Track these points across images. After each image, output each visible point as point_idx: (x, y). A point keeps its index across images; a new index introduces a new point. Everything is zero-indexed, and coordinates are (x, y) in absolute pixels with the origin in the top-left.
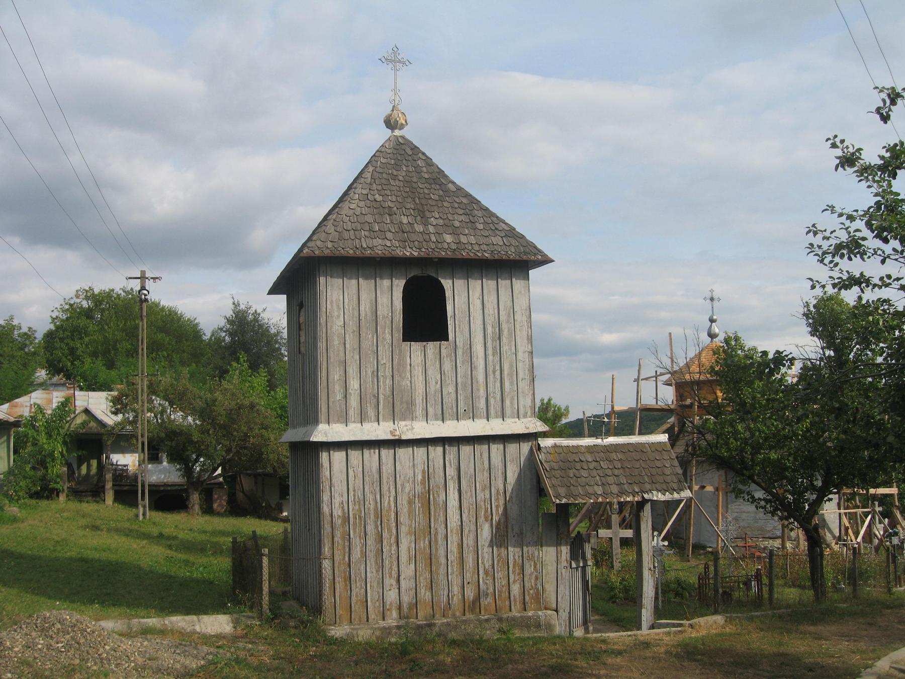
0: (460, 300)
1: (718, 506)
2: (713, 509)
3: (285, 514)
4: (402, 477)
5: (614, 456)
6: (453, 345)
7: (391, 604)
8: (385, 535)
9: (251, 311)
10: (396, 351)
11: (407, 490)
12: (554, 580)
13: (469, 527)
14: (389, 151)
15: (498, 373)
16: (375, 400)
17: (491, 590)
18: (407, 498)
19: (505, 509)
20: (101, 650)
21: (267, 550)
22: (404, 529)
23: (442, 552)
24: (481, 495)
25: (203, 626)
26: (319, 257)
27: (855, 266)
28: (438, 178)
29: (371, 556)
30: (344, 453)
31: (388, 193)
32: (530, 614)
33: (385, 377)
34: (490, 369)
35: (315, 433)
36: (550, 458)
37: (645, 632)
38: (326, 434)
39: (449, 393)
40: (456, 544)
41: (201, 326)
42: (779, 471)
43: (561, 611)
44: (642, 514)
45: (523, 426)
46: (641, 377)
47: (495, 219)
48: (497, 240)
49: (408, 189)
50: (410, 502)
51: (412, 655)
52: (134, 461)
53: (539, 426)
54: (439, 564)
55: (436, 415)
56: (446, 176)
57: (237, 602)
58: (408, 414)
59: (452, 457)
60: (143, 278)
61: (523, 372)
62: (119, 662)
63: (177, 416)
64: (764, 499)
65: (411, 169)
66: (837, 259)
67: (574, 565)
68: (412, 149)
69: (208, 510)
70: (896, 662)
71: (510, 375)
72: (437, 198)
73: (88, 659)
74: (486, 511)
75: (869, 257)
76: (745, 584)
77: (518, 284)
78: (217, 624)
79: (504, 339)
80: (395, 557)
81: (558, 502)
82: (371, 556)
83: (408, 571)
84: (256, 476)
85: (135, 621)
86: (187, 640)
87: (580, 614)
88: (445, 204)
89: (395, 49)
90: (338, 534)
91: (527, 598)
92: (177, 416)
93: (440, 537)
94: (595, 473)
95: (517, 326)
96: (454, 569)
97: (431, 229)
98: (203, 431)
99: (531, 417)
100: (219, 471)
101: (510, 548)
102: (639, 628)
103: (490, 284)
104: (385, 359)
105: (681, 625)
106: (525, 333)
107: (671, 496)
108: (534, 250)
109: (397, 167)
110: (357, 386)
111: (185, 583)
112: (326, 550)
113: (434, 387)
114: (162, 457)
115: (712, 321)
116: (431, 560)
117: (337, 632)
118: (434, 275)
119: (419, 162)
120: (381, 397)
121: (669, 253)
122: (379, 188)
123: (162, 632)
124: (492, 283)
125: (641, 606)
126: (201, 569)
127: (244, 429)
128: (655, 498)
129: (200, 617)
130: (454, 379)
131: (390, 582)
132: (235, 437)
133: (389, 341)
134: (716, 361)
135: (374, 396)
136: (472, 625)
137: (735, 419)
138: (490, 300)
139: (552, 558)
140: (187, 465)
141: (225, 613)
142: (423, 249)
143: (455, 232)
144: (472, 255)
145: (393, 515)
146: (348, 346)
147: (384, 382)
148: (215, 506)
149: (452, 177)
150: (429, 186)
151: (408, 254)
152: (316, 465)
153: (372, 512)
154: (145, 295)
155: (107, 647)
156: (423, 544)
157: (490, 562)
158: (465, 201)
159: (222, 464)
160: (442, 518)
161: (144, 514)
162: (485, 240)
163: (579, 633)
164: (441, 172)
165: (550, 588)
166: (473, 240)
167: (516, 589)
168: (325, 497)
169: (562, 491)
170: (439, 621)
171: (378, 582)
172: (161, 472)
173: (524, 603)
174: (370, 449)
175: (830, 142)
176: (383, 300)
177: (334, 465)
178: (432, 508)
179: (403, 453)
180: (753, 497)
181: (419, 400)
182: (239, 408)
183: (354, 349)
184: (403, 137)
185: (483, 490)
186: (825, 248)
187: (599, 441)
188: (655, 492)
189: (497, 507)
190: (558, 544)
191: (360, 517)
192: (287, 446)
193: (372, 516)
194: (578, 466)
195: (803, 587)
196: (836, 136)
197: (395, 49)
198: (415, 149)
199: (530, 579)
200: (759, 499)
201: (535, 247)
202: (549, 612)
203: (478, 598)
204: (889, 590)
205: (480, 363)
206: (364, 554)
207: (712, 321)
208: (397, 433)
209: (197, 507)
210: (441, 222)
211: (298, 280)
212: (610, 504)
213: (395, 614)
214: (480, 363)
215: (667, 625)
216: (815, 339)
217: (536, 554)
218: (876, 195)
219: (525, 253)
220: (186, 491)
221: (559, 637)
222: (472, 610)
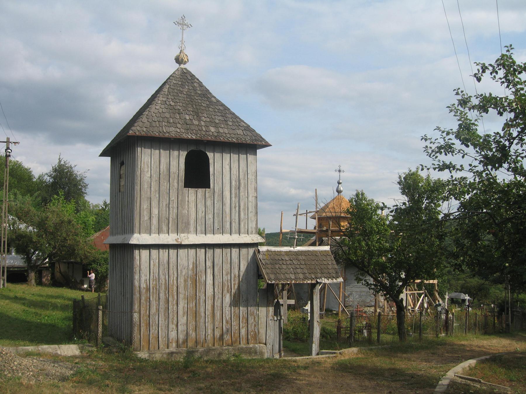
0: (218, 165)
1: (340, 287)
2: (337, 289)
3: (85, 286)
4: (181, 266)
5: (300, 257)
6: (212, 191)
7: (172, 339)
8: (170, 299)
10: (180, 193)
11: (183, 274)
12: (265, 328)
13: (218, 295)
14: (178, 77)
15: (237, 208)
16: (167, 221)
18: (183, 279)
19: (239, 286)
20: (12, 364)
21: (101, 307)
22: (181, 296)
23: (202, 310)
24: (225, 278)
25: (62, 351)
26: (138, 136)
27: (447, 159)
28: (206, 94)
29: (162, 311)
30: (148, 251)
31: (178, 101)
32: (251, 346)
33: (173, 208)
34: (233, 205)
35: (132, 239)
36: (265, 257)
37: (314, 356)
39: (210, 219)
40: (210, 305)
41: (33, 173)
42: (382, 268)
43: (268, 344)
44: (314, 291)
45: (250, 238)
46: (299, 213)
47: (238, 120)
48: (240, 132)
49: (189, 100)
50: (185, 281)
51: (190, 368)
55: (201, 230)
56: (210, 93)
57: (81, 337)
58: (186, 229)
60: (8, 142)
61: (251, 208)
62: (23, 371)
63: (23, 226)
64: (373, 284)
65: (191, 88)
66: (438, 154)
67: (275, 319)
68: (191, 76)
69: (39, 283)
70: (457, 373)
71: (244, 209)
72: (205, 105)
73: (5, 370)
74: (228, 287)
75: (456, 154)
76: (359, 331)
77: (251, 157)
78: (70, 350)
79: (242, 189)
80: (175, 312)
81: (270, 282)
82: (162, 311)
83: (183, 320)
84: (69, 263)
85: (20, 348)
86: (56, 359)
87: (277, 346)
88: (210, 109)
89: (183, 17)
90: (143, 298)
91: (249, 337)
92: (23, 226)
93: (202, 301)
94: (290, 267)
96: (209, 319)
97: (203, 123)
98: (39, 235)
99: (255, 234)
100: (47, 260)
102: (310, 354)
103: (235, 157)
104: (173, 197)
105: (335, 353)
106: (253, 186)
107: (332, 281)
108: (260, 139)
109: (182, 86)
111: (39, 326)
112: (136, 307)
113: (201, 214)
114: (11, 250)
115: (339, 183)
116: (196, 314)
117: (143, 355)
118: (203, 150)
119: (195, 84)
120: (171, 219)
122: (173, 98)
123: (39, 355)
124: (157, 151)
126: (46, 318)
127: (64, 235)
128: (323, 282)
129: (60, 346)
131: (172, 326)
132: (58, 239)
133: (176, 187)
134: (351, 206)
137: (356, 238)
138: (235, 166)
139: (265, 313)
140: (28, 256)
141: (74, 344)
143: (216, 126)
144: (226, 139)
145: (175, 288)
146: (152, 189)
147: (173, 211)
148: (44, 280)
149: (214, 94)
150: (201, 99)
151: (190, 137)
152: (132, 258)
154: (9, 153)
155: (16, 363)
156: (192, 305)
157: (230, 316)
158: (221, 108)
159: (49, 256)
160: (203, 290)
161: (4, 285)
162: (231, 132)
163: (277, 356)
164: (207, 91)
165: (262, 331)
166: (226, 131)
167: (243, 331)
168: (137, 277)
169: (272, 276)
171: (165, 327)
172: (11, 258)
173: (248, 340)
175: (456, 91)
176: (174, 163)
177: (142, 258)
178: (198, 284)
179: (182, 252)
180: (367, 283)
181: (192, 222)
182: (62, 223)
183: (156, 191)
184: (185, 69)
185: (227, 275)
186: (433, 148)
187: (292, 249)
188: (323, 279)
189: (234, 284)
190: (268, 305)
192: (108, 246)
194: (281, 262)
195: (394, 334)
196: (459, 89)
197: (183, 17)
198: (193, 76)
200: (371, 284)
201: (261, 137)
203: (222, 336)
204: (437, 335)
206: (158, 310)
207: (339, 183)
208: (180, 240)
209: (33, 281)
210: (208, 120)
211: (122, 149)
212: (277, 284)
213: (174, 345)
215: (327, 353)
216: (404, 196)
218: (459, 120)
219: (256, 140)
220: (27, 271)
221: (268, 359)
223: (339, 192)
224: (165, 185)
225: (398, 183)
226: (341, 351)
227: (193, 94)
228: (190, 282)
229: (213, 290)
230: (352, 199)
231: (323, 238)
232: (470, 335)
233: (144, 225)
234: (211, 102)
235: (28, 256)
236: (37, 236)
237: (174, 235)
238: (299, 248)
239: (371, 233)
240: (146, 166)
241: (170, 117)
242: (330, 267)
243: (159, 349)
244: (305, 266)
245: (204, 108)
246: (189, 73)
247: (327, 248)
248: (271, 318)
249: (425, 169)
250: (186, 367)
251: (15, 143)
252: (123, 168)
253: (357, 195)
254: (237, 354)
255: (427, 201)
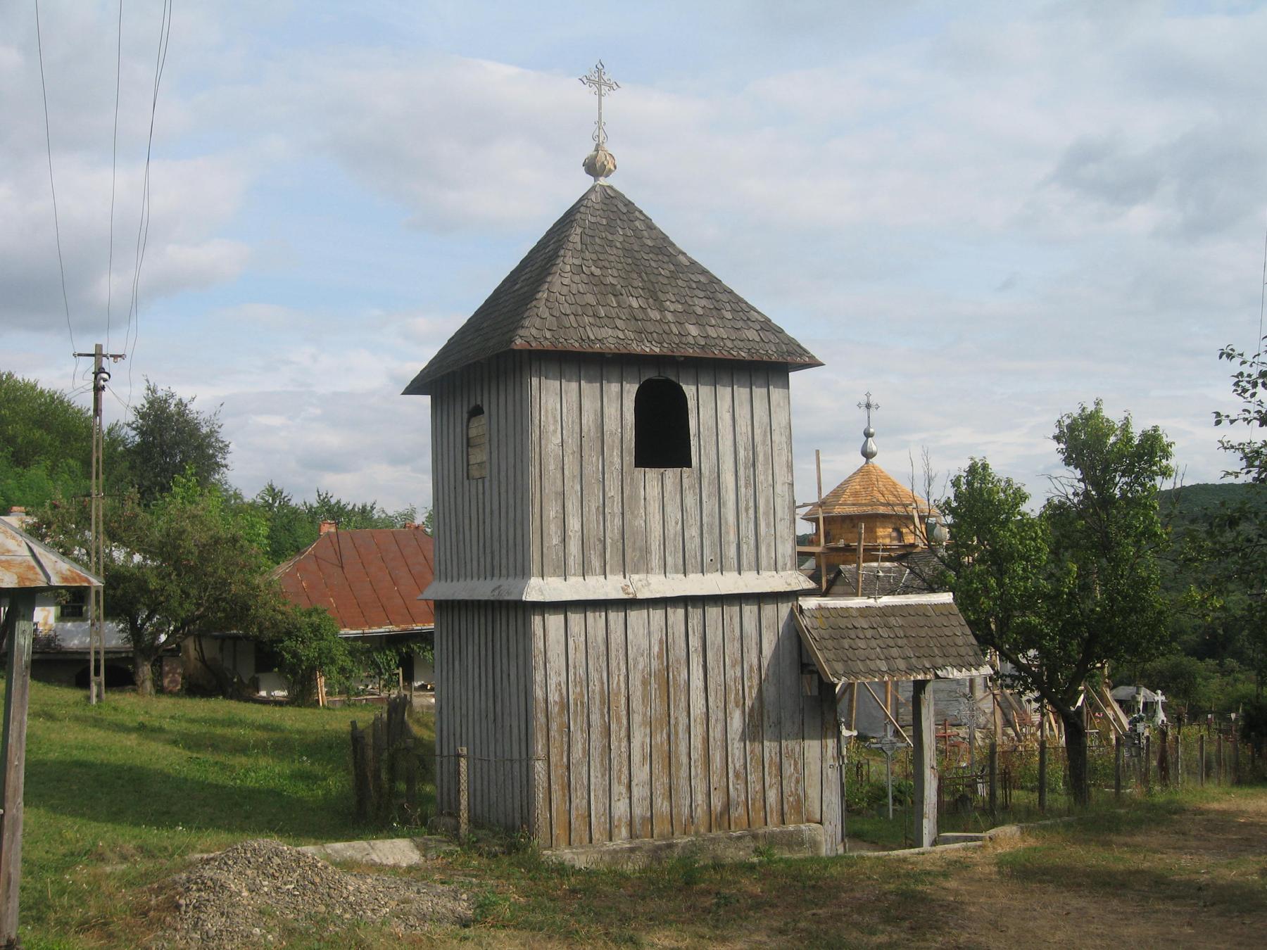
0: (706, 413)
5: (892, 621)
7: (620, 819)
8: (614, 727)
9: (173, 402)
10: (627, 481)
11: (640, 667)
14: (597, 206)
15: (751, 511)
16: (600, 546)
17: (743, 797)
19: (760, 690)
22: (637, 719)
24: (730, 673)
28: (663, 247)
30: (562, 617)
31: (607, 265)
32: (791, 827)
34: (742, 505)
36: (817, 623)
37: (926, 845)
38: (541, 590)
40: (700, 737)
43: (827, 823)
47: (744, 306)
48: (752, 334)
49: (630, 261)
50: (645, 683)
52: (46, 618)
53: (797, 580)
54: (679, 765)
55: (675, 566)
58: (643, 565)
59: (695, 622)
60: (98, 355)
64: (1010, 676)
65: (630, 233)
69: (160, 690)
71: (766, 514)
72: (668, 274)
74: (737, 694)
77: (776, 393)
79: (760, 467)
80: (625, 755)
84: (223, 639)
90: (554, 726)
91: (786, 807)
94: (874, 643)
95: (775, 449)
96: (698, 770)
97: (670, 317)
101: (766, 743)
102: (920, 844)
103: (742, 392)
104: (613, 491)
105: (977, 839)
106: (784, 459)
109: (610, 227)
110: (577, 527)
112: (540, 748)
113: (673, 528)
115: (868, 435)
118: (674, 379)
119: (637, 223)
120: (608, 541)
121: (945, 356)
124: (574, 385)
125: (921, 816)
129: (372, 842)
130: (698, 518)
131: (619, 789)
133: (618, 466)
135: (599, 540)
136: (722, 845)
138: (743, 413)
140: (133, 622)
142: (612, 335)
145: (623, 700)
147: (612, 522)
148: (166, 682)
149: (680, 245)
153: (597, 697)
154: (105, 380)
156: (660, 738)
158: (703, 279)
160: (683, 704)
161: (98, 696)
165: (813, 793)
167: (772, 796)
168: (539, 677)
170: (681, 840)
173: (782, 814)
174: (594, 612)
176: (611, 411)
178: (672, 690)
179: (636, 617)
181: (655, 546)
182: (216, 542)
184: (611, 187)
185: (733, 666)
187: (871, 602)
189: (750, 687)
190: (823, 736)
191: (582, 703)
193: (597, 702)
198: (629, 204)
199: (789, 782)
201: (799, 346)
202: (814, 825)
203: (727, 806)
205: (730, 497)
207: (868, 435)
209: (148, 684)
210: (680, 307)
213: (624, 832)
214: (730, 497)
215: (956, 840)
216: (1072, 468)
217: (797, 749)
219: (789, 353)
220: (131, 660)
222: (720, 827)
223: (868, 455)
224: (592, 460)
225: (1055, 437)
226: (992, 832)
227: (636, 248)
228: (654, 686)
229: (703, 702)
230: (958, 478)
231: (842, 567)
232: (1212, 788)
233: (552, 555)
234: (677, 264)
235: (133, 622)
236: (158, 576)
237: (616, 577)
238: (886, 600)
239: (1010, 557)
240: (551, 420)
241: (598, 303)
242: (960, 641)
243: (591, 841)
244: (905, 641)
245: (666, 281)
246: (619, 196)
247: (946, 598)
248: (831, 762)
249: (1225, 422)
250: (681, 881)
251: (115, 357)
252: (475, 422)
253: (972, 470)
254: (762, 848)
255: (1123, 480)
